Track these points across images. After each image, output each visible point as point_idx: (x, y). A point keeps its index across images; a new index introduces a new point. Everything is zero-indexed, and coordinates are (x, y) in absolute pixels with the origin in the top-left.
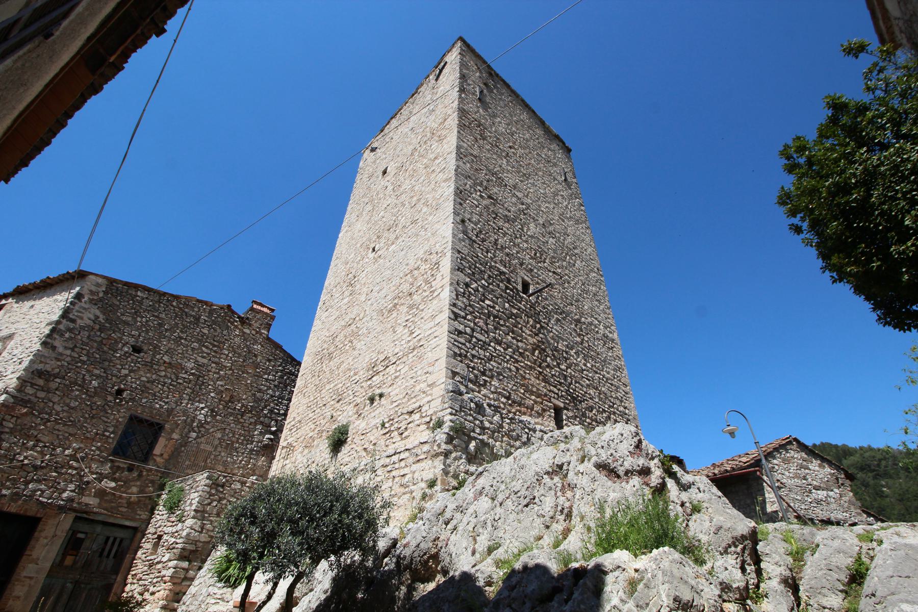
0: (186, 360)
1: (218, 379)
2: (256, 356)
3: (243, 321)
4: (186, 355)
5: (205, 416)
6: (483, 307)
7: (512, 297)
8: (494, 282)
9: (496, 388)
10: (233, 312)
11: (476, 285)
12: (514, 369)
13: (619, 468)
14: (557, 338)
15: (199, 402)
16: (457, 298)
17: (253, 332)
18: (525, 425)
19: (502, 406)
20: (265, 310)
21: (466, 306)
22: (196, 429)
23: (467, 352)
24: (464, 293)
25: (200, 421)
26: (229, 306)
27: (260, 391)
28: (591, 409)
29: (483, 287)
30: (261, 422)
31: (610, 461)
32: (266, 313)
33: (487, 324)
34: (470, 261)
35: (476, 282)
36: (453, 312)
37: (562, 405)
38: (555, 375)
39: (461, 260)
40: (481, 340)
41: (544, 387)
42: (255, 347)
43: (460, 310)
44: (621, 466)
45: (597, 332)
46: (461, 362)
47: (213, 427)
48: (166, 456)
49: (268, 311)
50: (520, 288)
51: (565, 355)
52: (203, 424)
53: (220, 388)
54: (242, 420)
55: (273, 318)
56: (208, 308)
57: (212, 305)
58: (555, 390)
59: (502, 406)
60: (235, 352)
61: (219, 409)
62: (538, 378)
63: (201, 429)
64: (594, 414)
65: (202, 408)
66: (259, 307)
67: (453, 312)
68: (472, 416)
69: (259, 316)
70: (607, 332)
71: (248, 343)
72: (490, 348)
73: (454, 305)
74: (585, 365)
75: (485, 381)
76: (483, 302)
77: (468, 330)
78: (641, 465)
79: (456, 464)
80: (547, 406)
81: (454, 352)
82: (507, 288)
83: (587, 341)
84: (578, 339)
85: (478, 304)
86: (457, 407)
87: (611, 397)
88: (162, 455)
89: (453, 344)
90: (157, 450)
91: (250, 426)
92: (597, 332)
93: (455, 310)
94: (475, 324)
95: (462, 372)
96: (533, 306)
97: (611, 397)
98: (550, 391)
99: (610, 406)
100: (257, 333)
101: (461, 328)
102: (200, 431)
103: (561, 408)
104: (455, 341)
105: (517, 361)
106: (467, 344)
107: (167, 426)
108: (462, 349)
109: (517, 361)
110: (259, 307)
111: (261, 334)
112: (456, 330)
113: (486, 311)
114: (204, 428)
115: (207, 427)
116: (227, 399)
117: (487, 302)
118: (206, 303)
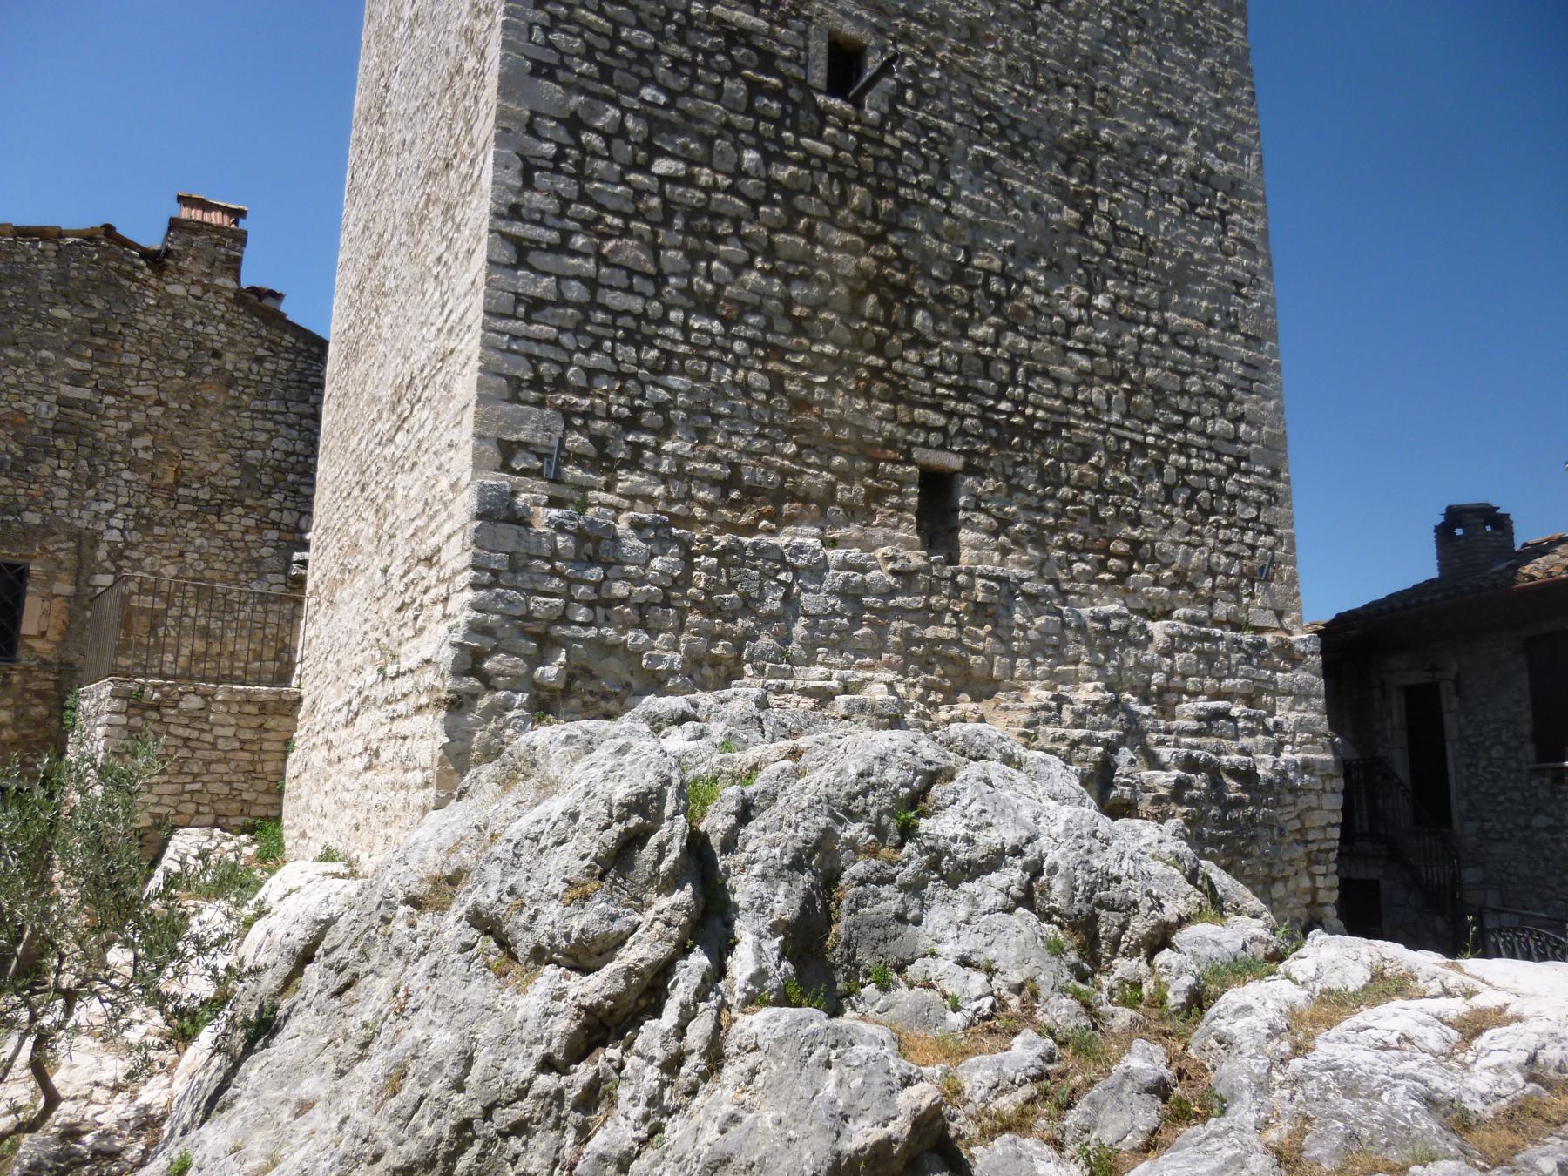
0: (32, 400)
1: (133, 433)
2: (216, 354)
3: (155, 260)
4: (29, 387)
5: (122, 531)
6: (639, 193)
7: (778, 123)
8: (695, 79)
9: (680, 460)
10: (125, 243)
11: (613, 112)
12: (757, 379)
13: (519, 935)
14: (973, 234)
15: (97, 498)
16: (528, 183)
17: (197, 290)
18: (782, 560)
19: (699, 512)
20: (215, 218)
21: (565, 203)
22: (107, 564)
23: (565, 366)
24: (560, 156)
25: (112, 544)
26: (108, 230)
27: (252, 445)
28: (1084, 451)
29: (647, 113)
30: (273, 523)
31: (502, 909)
32: (218, 229)
33: (655, 249)
34: (586, 26)
35: (615, 102)
36: (504, 236)
37: (956, 462)
38: (942, 368)
39: (546, 30)
40: (627, 313)
41: (893, 418)
42: (210, 330)
43: (540, 223)
44: (527, 929)
45: (1165, 169)
46: (540, 404)
47: (149, 554)
48: (53, 635)
49: (226, 221)
50: (818, 74)
51: (995, 285)
52: (122, 551)
53: (141, 454)
54: (220, 526)
55: (241, 238)
56: (51, 246)
57: (61, 234)
58: (939, 420)
59: (699, 512)
60: (160, 357)
61: (153, 507)
62: (867, 394)
63: (121, 563)
64: (1095, 467)
65: (111, 513)
66: (197, 214)
67: (504, 236)
68: (561, 576)
69: (199, 240)
70: (1209, 157)
71: (188, 324)
72: (670, 331)
73: (515, 212)
74: (1085, 304)
75: (637, 448)
76: (645, 169)
77: (575, 291)
78: (575, 935)
79: (492, 725)
80: (893, 477)
81: (509, 378)
82: (755, 88)
83: (1109, 215)
84: (1070, 215)
85: (623, 182)
86: (499, 560)
87: (1183, 392)
88: (43, 634)
89: (509, 350)
90: (29, 624)
91: (248, 538)
92: (1165, 169)
93: (517, 229)
94: (602, 260)
95: (539, 438)
96: (871, 136)
97: (1183, 392)
98: (911, 425)
99: (1170, 428)
100: (206, 290)
101: (544, 287)
102: (119, 569)
103: (955, 472)
104: (515, 338)
105: (777, 352)
106: (566, 339)
107: (34, 568)
108: (540, 359)
109: (777, 352)
110: (197, 214)
111: (218, 291)
112: (519, 298)
113: (655, 202)
114: (128, 558)
115: (135, 555)
116: (170, 479)
117: (662, 166)
118: (42, 234)
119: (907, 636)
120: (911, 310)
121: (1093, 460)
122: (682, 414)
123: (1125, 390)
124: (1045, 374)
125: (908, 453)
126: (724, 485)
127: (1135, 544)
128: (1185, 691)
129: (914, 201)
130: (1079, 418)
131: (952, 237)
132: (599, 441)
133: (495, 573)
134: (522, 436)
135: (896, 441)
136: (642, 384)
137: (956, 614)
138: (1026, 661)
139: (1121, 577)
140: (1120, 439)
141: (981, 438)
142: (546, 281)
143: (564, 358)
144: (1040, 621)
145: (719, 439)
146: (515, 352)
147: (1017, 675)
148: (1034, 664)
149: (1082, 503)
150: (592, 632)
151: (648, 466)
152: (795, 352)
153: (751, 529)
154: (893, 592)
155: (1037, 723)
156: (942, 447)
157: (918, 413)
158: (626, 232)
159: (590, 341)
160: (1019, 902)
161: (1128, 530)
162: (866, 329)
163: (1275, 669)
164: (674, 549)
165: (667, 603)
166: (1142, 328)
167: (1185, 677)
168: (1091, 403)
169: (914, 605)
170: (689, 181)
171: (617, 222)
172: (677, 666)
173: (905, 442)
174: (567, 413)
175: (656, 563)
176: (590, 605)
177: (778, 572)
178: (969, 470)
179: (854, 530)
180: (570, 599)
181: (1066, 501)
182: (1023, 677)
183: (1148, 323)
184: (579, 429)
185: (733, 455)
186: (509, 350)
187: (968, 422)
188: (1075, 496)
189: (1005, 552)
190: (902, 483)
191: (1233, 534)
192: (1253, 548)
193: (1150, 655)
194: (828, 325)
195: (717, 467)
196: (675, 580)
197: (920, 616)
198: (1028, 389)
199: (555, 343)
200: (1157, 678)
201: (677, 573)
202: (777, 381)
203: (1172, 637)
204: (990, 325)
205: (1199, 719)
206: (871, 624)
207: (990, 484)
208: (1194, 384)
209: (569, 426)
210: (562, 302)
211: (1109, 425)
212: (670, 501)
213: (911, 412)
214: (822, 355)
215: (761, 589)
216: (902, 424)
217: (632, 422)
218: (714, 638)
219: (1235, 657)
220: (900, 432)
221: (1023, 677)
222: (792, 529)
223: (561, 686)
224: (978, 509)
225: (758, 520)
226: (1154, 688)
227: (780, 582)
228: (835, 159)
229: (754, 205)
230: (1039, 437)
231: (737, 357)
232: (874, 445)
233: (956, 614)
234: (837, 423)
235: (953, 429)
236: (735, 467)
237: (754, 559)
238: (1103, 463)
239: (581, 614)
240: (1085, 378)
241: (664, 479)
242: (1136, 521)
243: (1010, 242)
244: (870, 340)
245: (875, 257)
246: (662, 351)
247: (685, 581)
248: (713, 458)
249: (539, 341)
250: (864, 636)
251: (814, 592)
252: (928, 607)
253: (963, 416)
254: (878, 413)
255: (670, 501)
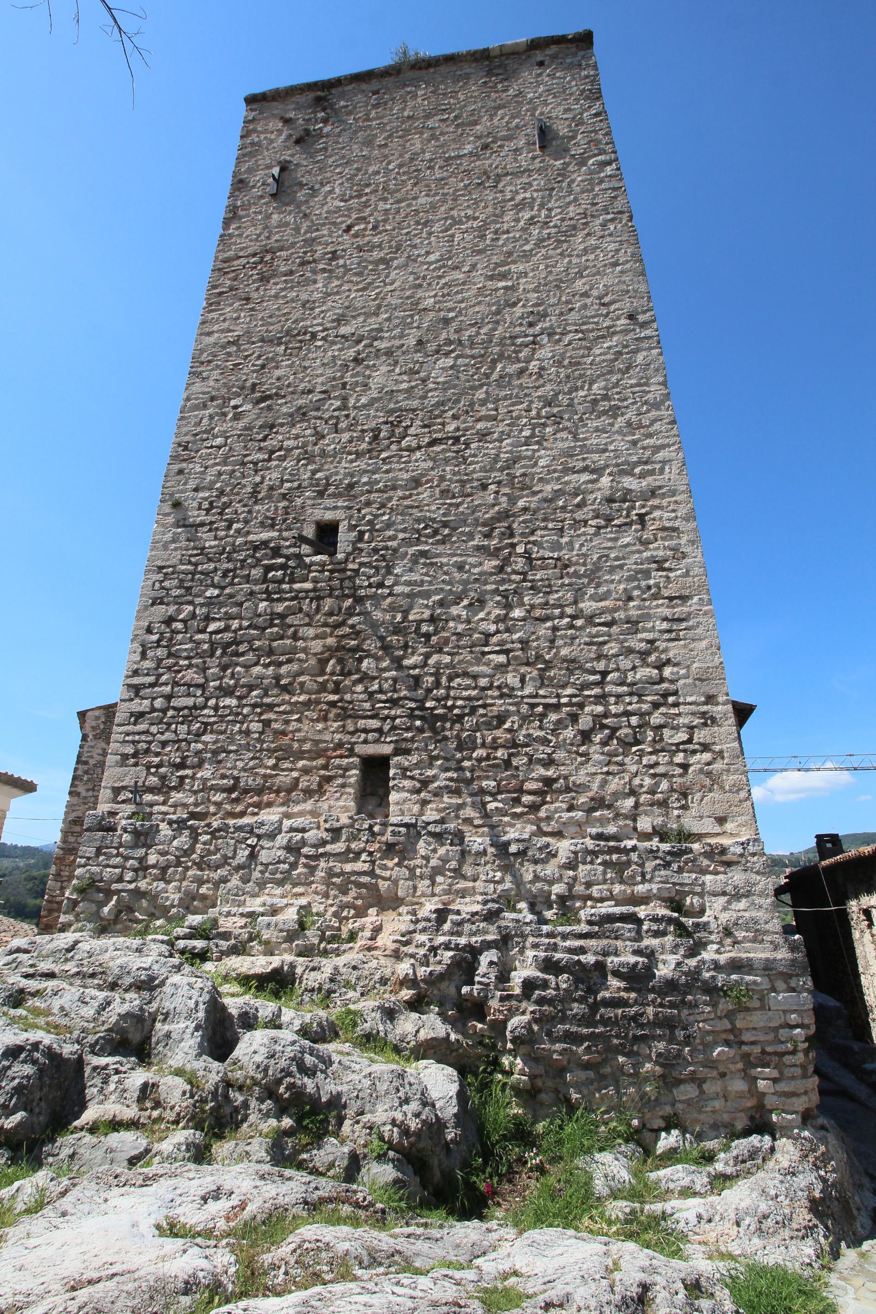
9: (205, 780)
12: (256, 726)
19: (212, 809)
33: (204, 669)
37: (387, 749)
41: (343, 729)
43: (147, 675)
62: (325, 719)
80: (339, 767)
81: (122, 755)
89: (125, 742)
104: (128, 734)
112: (132, 714)
117: (212, 627)
119: (331, 873)
120: (360, 660)
121: (507, 725)
122: (209, 755)
123: (539, 669)
124: (466, 674)
125: (351, 750)
126: (229, 790)
127: (548, 782)
128: (590, 897)
129: (366, 596)
130: (493, 698)
131: (392, 608)
132: (163, 778)
133: (88, 859)
134: (123, 784)
135: (344, 744)
136: (189, 743)
137: (370, 854)
138: (427, 882)
139: (534, 808)
140: (533, 706)
141: (408, 729)
142: (145, 702)
143: (150, 738)
144: (442, 851)
145: (229, 765)
146: (127, 742)
147: (419, 893)
148: (433, 883)
149: (495, 758)
150: (132, 886)
151: (187, 787)
152: (279, 705)
153: (242, 814)
154: (324, 843)
155: (414, 931)
156: (377, 741)
157: (361, 723)
158: (190, 666)
159: (165, 726)
160: (726, 1016)
161: (541, 771)
162: (328, 680)
163: (704, 872)
164: (186, 832)
165: (178, 864)
166: (556, 621)
167: (589, 885)
168: (507, 686)
169: (338, 851)
170: (227, 629)
171: (186, 662)
172: (176, 902)
173: (349, 743)
174: (148, 767)
175: (175, 843)
176: (135, 870)
177: (247, 839)
178: (397, 752)
179: (308, 806)
180: (124, 868)
181: (480, 760)
182: (423, 895)
183: (562, 616)
184: (153, 774)
185: (235, 773)
186: (125, 742)
187: (398, 721)
188: (488, 755)
189: (424, 803)
190: (346, 770)
191: (663, 758)
192: (685, 767)
193: (550, 869)
194: (302, 684)
195: (225, 781)
196: (185, 851)
197: (343, 857)
198: (449, 688)
199: (147, 732)
200: (558, 889)
201: (186, 847)
202: (267, 723)
203: (575, 853)
204: (420, 655)
205: (590, 923)
206: (305, 866)
207: (414, 758)
208: (612, 648)
209: (149, 773)
210: (153, 710)
211: (522, 697)
212: (196, 805)
213: (356, 724)
214: (297, 702)
215: (235, 851)
216: (349, 733)
217: (182, 766)
218: (201, 882)
219: (649, 865)
220: (346, 738)
221: (423, 895)
222: (268, 810)
223: (112, 917)
224: (405, 777)
225: (247, 808)
226: (553, 897)
227: (249, 846)
228: (315, 590)
229: (525, 574)
230: (460, 718)
231: (245, 716)
232: (326, 750)
233: (370, 854)
234: (302, 741)
235: (386, 727)
236: (237, 779)
237: (233, 833)
238: (516, 726)
239: (129, 876)
240: (502, 668)
241: (195, 793)
242: (549, 762)
243: (438, 597)
244: (331, 686)
245: (337, 636)
246: (203, 723)
247: (192, 849)
248: (224, 777)
249: (139, 733)
250: (299, 875)
251: (269, 849)
252: (349, 850)
253: (394, 719)
254: (332, 729)
255: (196, 805)
